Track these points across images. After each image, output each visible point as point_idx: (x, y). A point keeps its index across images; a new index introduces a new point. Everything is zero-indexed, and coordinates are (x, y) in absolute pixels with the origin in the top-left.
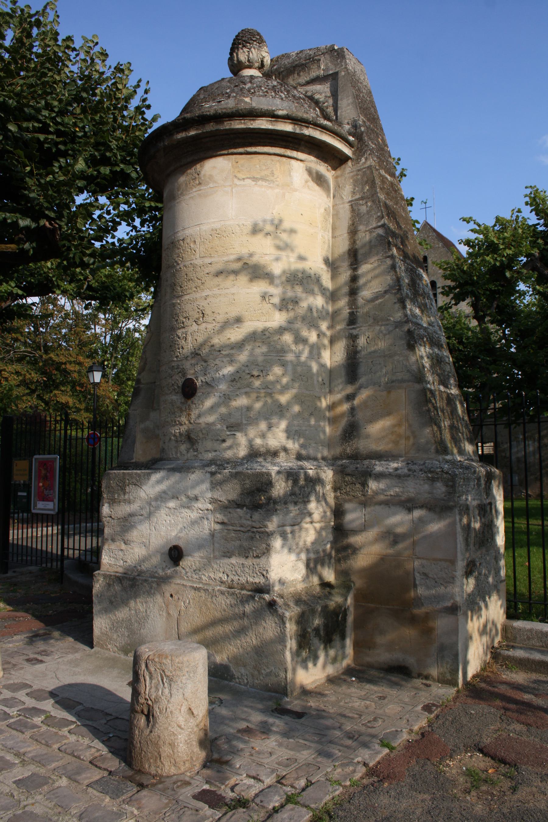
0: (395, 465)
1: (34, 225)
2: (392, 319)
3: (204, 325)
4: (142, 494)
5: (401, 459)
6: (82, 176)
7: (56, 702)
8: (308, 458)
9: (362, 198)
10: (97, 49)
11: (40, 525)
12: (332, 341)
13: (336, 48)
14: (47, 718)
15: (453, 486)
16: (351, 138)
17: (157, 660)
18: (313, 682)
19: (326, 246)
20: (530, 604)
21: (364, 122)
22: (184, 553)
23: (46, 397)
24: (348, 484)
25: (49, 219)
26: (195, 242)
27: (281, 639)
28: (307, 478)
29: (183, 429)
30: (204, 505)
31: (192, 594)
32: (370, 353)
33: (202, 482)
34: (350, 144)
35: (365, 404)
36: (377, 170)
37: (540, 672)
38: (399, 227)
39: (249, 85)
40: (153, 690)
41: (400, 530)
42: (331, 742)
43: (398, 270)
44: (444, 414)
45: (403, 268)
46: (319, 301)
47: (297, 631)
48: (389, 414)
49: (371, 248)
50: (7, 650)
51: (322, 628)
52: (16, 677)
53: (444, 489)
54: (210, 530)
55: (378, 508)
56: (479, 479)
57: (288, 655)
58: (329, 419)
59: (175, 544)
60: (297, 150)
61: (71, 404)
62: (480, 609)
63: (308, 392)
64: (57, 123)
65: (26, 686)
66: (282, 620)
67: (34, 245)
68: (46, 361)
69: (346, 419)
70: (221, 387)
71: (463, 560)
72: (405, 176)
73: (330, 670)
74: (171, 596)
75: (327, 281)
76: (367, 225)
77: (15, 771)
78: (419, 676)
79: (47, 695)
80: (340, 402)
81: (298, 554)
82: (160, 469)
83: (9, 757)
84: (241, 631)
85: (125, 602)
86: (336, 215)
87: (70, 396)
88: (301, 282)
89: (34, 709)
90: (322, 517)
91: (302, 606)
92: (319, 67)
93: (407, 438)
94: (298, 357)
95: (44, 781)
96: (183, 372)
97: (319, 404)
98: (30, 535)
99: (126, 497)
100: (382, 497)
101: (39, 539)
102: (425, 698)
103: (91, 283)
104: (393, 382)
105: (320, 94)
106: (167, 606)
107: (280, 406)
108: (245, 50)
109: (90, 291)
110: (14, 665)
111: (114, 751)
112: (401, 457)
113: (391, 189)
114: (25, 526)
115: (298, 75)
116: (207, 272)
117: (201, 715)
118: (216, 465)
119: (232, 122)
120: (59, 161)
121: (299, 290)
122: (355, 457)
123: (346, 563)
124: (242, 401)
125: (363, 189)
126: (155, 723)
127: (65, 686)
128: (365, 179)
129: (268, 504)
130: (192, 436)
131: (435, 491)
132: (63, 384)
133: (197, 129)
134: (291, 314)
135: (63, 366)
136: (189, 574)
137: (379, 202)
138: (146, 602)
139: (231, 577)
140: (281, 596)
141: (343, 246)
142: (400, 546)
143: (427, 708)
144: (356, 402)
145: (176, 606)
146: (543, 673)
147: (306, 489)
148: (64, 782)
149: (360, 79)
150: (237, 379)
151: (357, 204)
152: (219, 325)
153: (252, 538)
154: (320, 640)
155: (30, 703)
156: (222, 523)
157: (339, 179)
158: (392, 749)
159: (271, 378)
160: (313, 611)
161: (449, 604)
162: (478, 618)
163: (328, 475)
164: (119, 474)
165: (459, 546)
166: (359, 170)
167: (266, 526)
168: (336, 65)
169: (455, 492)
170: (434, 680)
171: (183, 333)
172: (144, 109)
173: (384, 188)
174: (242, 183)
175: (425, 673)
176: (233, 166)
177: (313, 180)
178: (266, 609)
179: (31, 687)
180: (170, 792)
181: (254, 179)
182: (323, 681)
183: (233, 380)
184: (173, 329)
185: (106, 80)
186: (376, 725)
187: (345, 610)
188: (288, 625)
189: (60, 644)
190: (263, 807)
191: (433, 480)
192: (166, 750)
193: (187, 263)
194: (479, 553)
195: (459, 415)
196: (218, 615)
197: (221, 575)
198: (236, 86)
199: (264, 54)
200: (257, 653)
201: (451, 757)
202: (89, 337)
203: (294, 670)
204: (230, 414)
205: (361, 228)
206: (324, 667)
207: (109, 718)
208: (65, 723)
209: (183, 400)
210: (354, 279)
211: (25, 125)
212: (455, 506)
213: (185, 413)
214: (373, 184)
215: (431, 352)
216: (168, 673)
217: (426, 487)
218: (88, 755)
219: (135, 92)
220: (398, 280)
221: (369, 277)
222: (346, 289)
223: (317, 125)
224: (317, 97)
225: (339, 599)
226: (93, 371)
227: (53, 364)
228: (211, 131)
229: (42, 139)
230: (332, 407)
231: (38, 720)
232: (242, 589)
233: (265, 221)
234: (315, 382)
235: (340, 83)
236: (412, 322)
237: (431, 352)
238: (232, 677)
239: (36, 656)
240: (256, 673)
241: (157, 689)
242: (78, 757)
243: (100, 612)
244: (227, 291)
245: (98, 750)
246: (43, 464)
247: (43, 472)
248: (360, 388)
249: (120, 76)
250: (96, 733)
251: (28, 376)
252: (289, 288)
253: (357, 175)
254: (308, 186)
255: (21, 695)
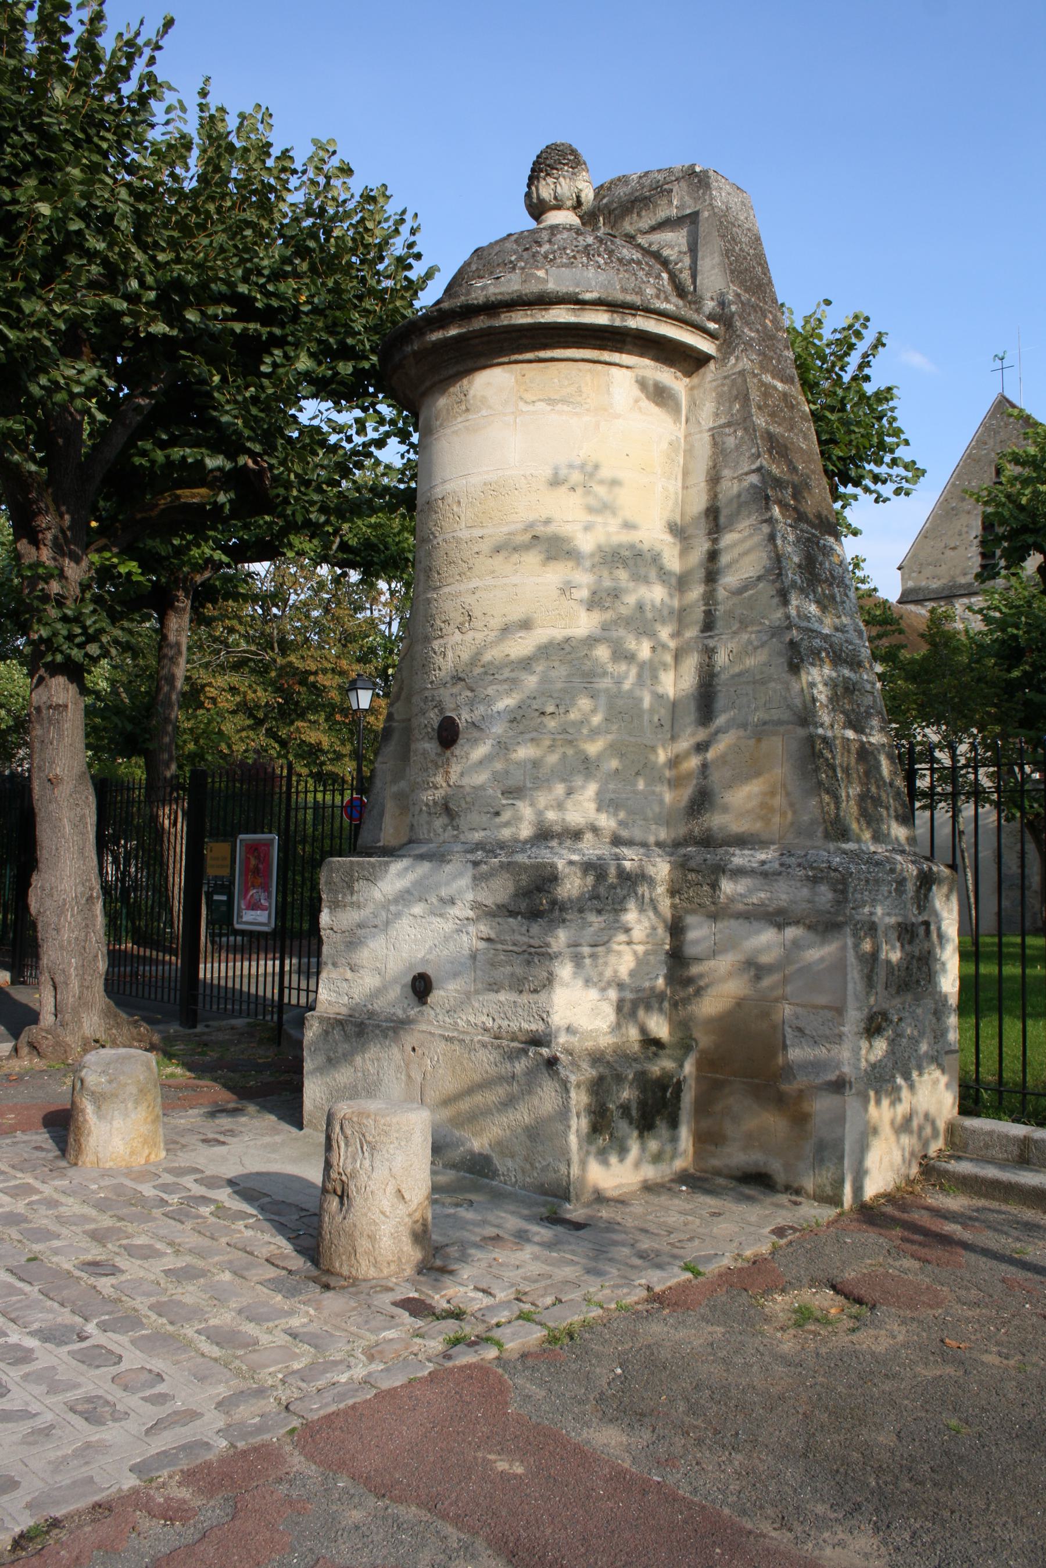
0: (762, 856)
1: (229, 465)
2: (767, 622)
3: (471, 634)
4: (377, 895)
5: (773, 847)
6: (307, 376)
7: (235, 1192)
8: (630, 843)
9: (729, 424)
10: (335, 162)
11: (262, 956)
12: (678, 656)
13: (698, 169)
14: (218, 1208)
15: (844, 892)
16: (712, 326)
17: (355, 1119)
18: (616, 1187)
19: (671, 503)
20: (1001, 1093)
21: (738, 295)
22: (434, 984)
23: (283, 733)
24: (691, 884)
25: (253, 455)
26: (459, 502)
27: (563, 1114)
28: (622, 874)
29: (439, 794)
30: (462, 910)
31: (441, 1046)
32: (733, 677)
33: (461, 874)
34: (712, 335)
35: (723, 759)
36: (755, 375)
37: (993, 1198)
38: (794, 470)
39: (546, 247)
40: (349, 1161)
41: (765, 959)
42: (610, 1260)
43: (779, 542)
44: (848, 775)
45: (791, 538)
46: (657, 594)
47: (590, 1105)
48: (758, 774)
49: (740, 506)
50: (176, 1127)
51: (634, 1106)
52: (184, 1160)
53: (830, 895)
54: (470, 949)
55: (733, 923)
56: (901, 882)
57: (573, 1140)
58: (669, 781)
59: (420, 971)
60: (620, 351)
61: (325, 746)
62: (898, 1089)
63: (632, 739)
64: (268, 295)
65: (196, 1170)
66: (565, 1085)
67: (233, 496)
68: (282, 667)
69: (694, 782)
70: (494, 730)
71: (860, 1009)
72: (884, 345)
73: (649, 1172)
74: (414, 1049)
75: (673, 562)
76: (735, 468)
77: (165, 1260)
78: (788, 1189)
79: (224, 1183)
80: (687, 755)
81: (603, 990)
82: (404, 856)
83: (159, 1246)
84: (509, 1103)
85: (347, 1058)
86: (689, 452)
87: (324, 732)
88: (624, 562)
89: (203, 1197)
90: (648, 936)
91: (601, 1069)
92: (671, 202)
93: (783, 814)
94: (619, 683)
95: (203, 1273)
96: (440, 706)
97: (652, 757)
98: (246, 972)
99: (355, 898)
100: (740, 907)
101: (261, 979)
102: (783, 1218)
103: (345, 539)
104: (765, 723)
105: (672, 247)
106: (407, 1065)
107: (586, 759)
108: (550, 180)
109: (343, 552)
110: (184, 1146)
111: (300, 1251)
112: (773, 843)
113: (783, 404)
114: (238, 957)
115: (639, 215)
116: (476, 550)
117: (416, 1202)
118: (483, 849)
119: (513, 314)
120: (272, 355)
121: (623, 575)
122: (707, 841)
123: (685, 1009)
124: (524, 752)
125: (731, 408)
126: (350, 1205)
127: (251, 1174)
128: (735, 392)
129: (552, 910)
130: (451, 806)
131: (817, 899)
132: (313, 707)
133: (460, 326)
134: (608, 615)
135: (312, 678)
136: (440, 1017)
137: (755, 431)
138: (378, 1060)
139: (499, 1021)
140: (569, 1052)
141: (699, 502)
142: (766, 982)
143: (780, 1232)
144: (710, 755)
145: (420, 1065)
146: (997, 1200)
147: (618, 890)
148: (227, 1276)
149: (737, 219)
150: (519, 718)
151: (721, 434)
152: (493, 634)
153: (529, 963)
154: (631, 1123)
155: (198, 1190)
156: (488, 940)
157: (696, 392)
158: (697, 1274)
159: (573, 716)
160: (619, 1079)
161: (832, 1077)
162: (893, 1104)
163: (661, 869)
164: (344, 863)
165: (850, 986)
166: (725, 378)
167: (548, 945)
168: (696, 199)
169: (846, 900)
170: (808, 1197)
171: (440, 646)
172: (411, 260)
173: (766, 405)
174: (531, 408)
175: (796, 1185)
176: (517, 381)
177: (648, 398)
178: (544, 1071)
179: (202, 1172)
180: (363, 1296)
181: (551, 402)
182: (635, 1188)
183: (513, 720)
184: (427, 640)
185: (347, 215)
186: (689, 1245)
187: (679, 1083)
188: (573, 1094)
189: (256, 1122)
190: (484, 1321)
191: (815, 881)
192: (363, 1244)
193: (448, 536)
194: (897, 1002)
195: (882, 778)
196: (477, 1078)
197: (484, 1018)
198: (526, 249)
199: (581, 185)
200: (529, 1137)
201: (783, 1291)
202: (359, 625)
203: (583, 1163)
204: (507, 772)
205: (726, 473)
206: (637, 1165)
207: (303, 1214)
208: (242, 1215)
209: (439, 750)
210: (713, 556)
211: (210, 311)
212: (845, 923)
213: (441, 770)
214: (745, 399)
215: (834, 674)
216: (369, 1138)
217: (805, 892)
218: (264, 1252)
219: (397, 231)
220: (778, 559)
221: (735, 553)
222: (701, 574)
223: (649, 311)
224: (666, 252)
225: (669, 1064)
226: (356, 689)
227: (294, 675)
228: (481, 329)
229: (238, 331)
230: (674, 762)
231: (205, 1210)
232: (512, 1040)
233: (571, 466)
234: (646, 723)
235: (701, 229)
236: (799, 628)
237: (834, 674)
238: (494, 1174)
239: (218, 1137)
240: (528, 1166)
241: (354, 1160)
242: (251, 1253)
243: (312, 1072)
244: (506, 581)
245: (280, 1247)
246: (253, 848)
247: (253, 862)
248: (717, 732)
249: (371, 208)
250: (281, 1228)
251: (251, 695)
252: (605, 573)
253: (723, 385)
254: (640, 408)
255: (188, 1181)
